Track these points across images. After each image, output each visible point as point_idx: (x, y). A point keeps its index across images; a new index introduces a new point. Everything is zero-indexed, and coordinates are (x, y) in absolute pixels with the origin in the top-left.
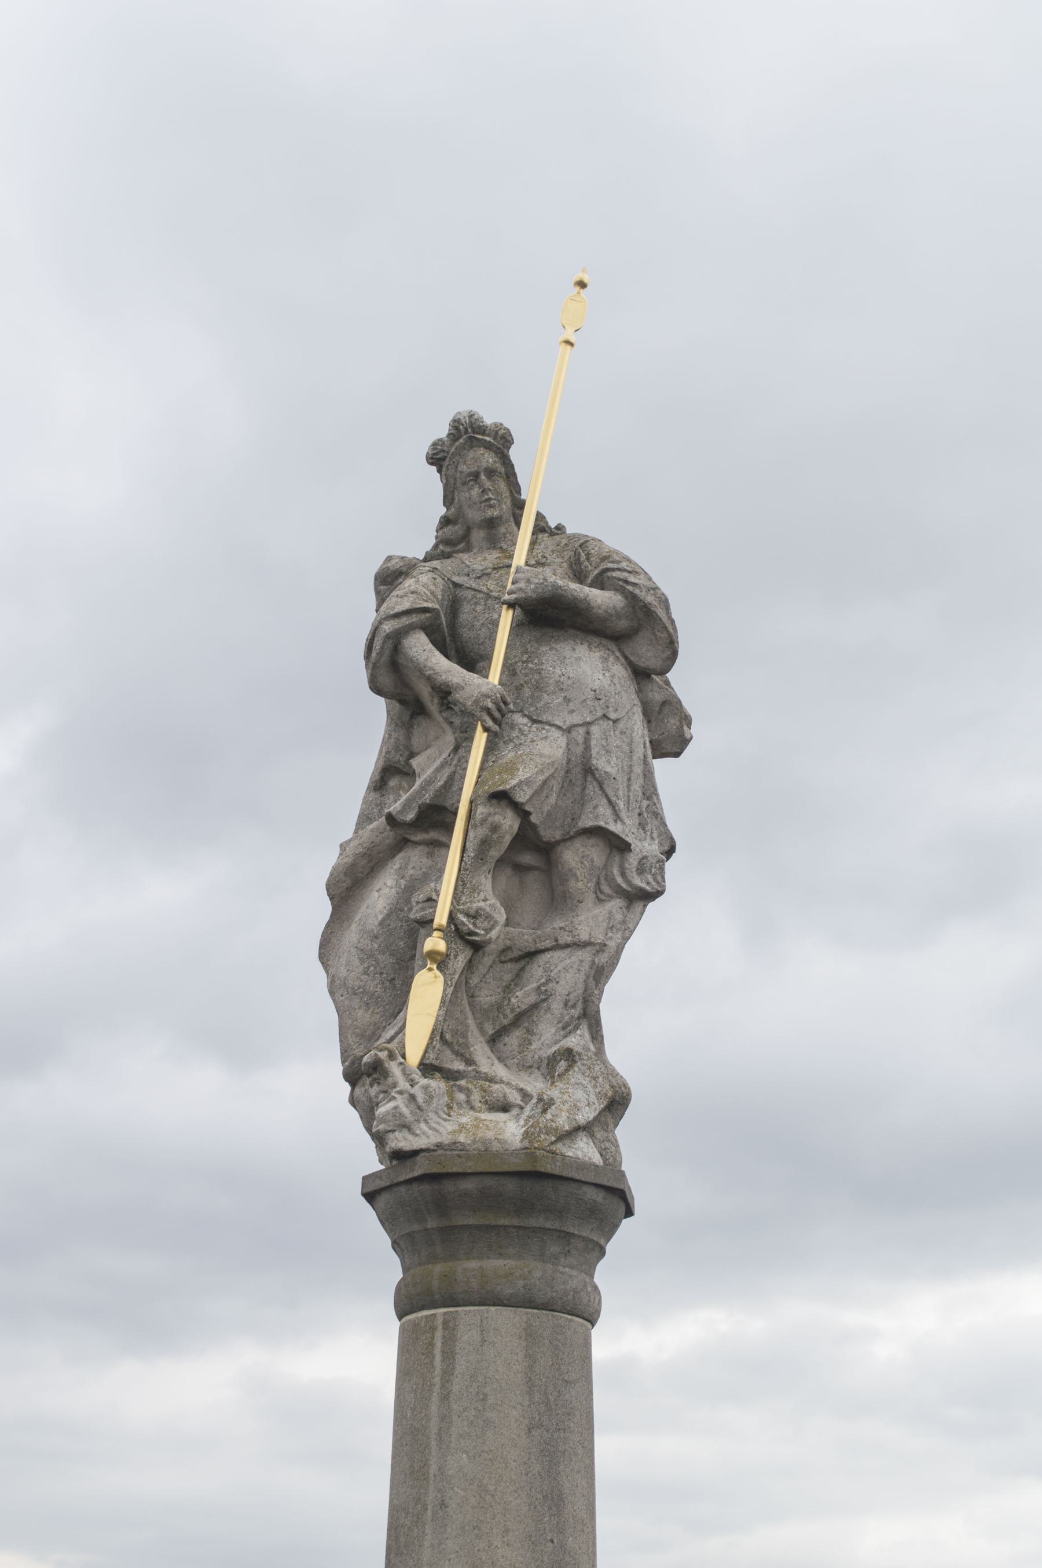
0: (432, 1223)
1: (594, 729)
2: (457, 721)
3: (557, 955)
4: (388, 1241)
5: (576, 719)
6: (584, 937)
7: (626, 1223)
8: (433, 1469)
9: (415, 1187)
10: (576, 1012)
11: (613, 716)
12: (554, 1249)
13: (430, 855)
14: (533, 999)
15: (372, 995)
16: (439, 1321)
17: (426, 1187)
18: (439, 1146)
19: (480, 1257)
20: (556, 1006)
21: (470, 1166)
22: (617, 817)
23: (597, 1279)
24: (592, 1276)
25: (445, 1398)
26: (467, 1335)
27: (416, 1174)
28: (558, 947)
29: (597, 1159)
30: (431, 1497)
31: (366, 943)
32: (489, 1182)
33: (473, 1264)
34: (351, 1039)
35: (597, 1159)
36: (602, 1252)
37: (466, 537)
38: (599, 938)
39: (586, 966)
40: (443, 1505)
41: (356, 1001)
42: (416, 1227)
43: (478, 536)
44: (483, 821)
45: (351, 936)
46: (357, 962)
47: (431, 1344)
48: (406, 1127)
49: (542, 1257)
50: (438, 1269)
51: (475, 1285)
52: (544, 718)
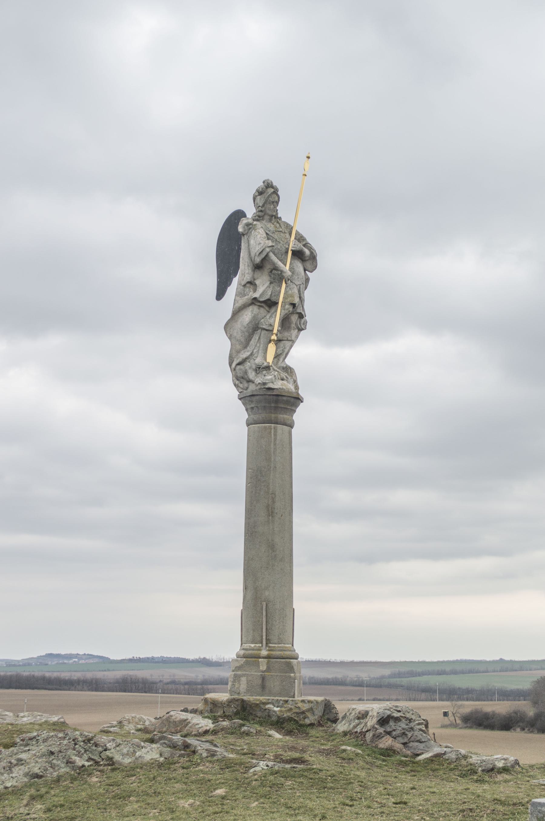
0: (273, 405)
2: (272, 276)
3: (287, 342)
7: (301, 404)
8: (273, 459)
9: (271, 397)
13: (259, 309)
14: (281, 352)
15: (242, 342)
16: (273, 427)
17: (275, 397)
18: (280, 388)
19: (282, 414)
21: (286, 394)
23: (293, 418)
24: (292, 416)
25: (275, 444)
26: (279, 432)
27: (274, 394)
28: (288, 340)
29: (294, 390)
30: (272, 465)
31: (243, 329)
32: (289, 398)
33: (281, 416)
34: (234, 352)
35: (294, 390)
36: (295, 411)
37: (263, 216)
40: (275, 467)
41: (237, 343)
42: (267, 405)
43: (267, 217)
44: (287, 309)
46: (240, 333)
47: (271, 432)
48: (273, 382)
50: (273, 415)
51: (282, 420)
52: (293, 281)
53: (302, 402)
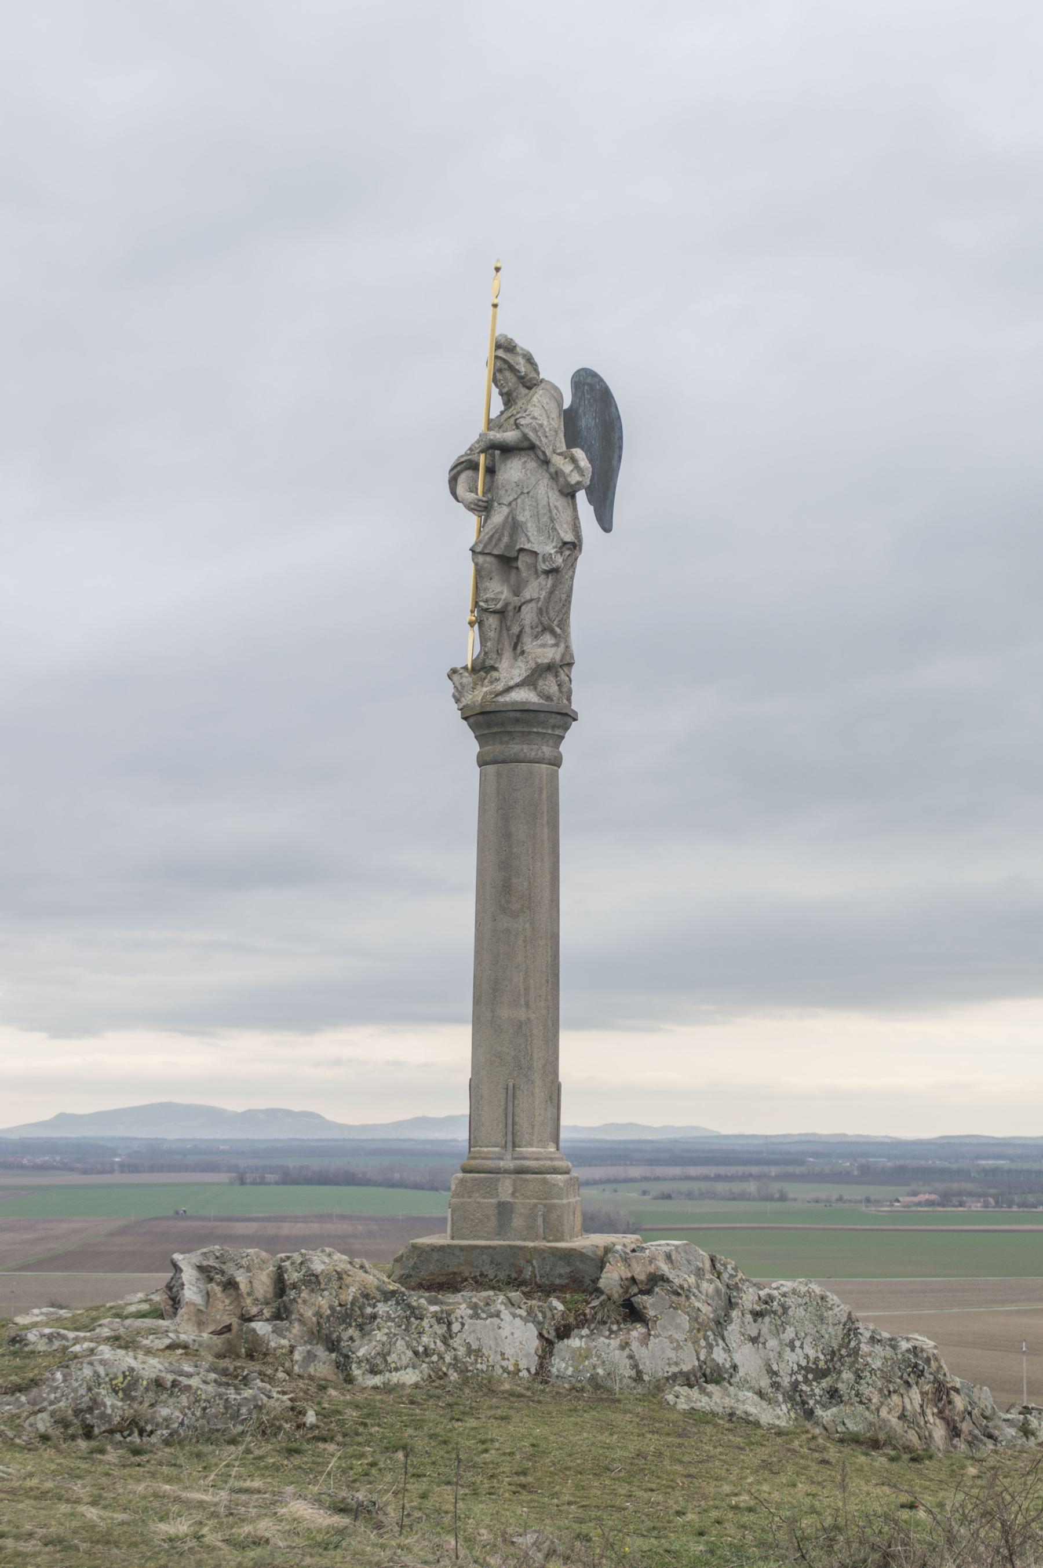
1: (519, 500)
4: (472, 735)
5: (511, 498)
6: (528, 597)
7: (574, 723)
10: (540, 629)
11: (526, 491)
12: (506, 738)
14: (518, 629)
20: (527, 629)
22: (529, 541)
36: (563, 737)
38: (536, 596)
39: (535, 609)
45: (566, 589)
49: (501, 743)
53: (575, 720)
